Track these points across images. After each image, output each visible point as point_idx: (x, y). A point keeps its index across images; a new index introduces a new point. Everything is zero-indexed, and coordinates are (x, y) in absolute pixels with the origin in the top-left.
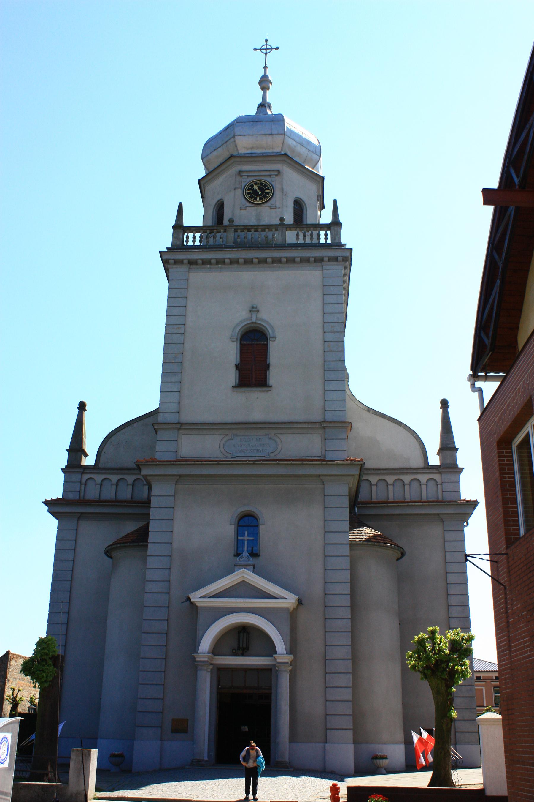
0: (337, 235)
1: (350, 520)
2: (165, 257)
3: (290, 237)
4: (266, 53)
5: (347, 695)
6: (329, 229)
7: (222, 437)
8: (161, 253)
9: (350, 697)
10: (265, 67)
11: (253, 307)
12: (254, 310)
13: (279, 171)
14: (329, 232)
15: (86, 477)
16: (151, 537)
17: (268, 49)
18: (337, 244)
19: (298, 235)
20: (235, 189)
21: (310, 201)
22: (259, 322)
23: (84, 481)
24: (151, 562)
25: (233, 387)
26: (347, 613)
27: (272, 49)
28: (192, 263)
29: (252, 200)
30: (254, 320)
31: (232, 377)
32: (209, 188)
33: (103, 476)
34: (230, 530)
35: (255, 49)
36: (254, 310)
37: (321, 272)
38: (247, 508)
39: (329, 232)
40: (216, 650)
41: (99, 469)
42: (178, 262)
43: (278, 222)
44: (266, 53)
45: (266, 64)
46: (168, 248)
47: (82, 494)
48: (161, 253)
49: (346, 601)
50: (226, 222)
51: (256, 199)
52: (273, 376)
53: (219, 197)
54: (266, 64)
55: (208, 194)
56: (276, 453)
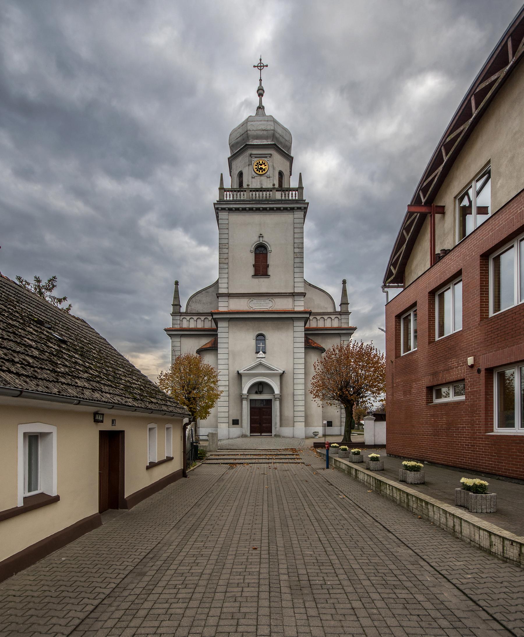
0: (301, 194)
1: (218, 343)
2: (216, 206)
3: (278, 195)
4: (261, 70)
5: (303, 409)
6: (297, 190)
7: (248, 299)
8: (214, 204)
9: (304, 410)
10: (261, 80)
11: (261, 235)
12: (261, 236)
13: (271, 155)
14: (297, 192)
15: (182, 317)
16: (219, 345)
17: (262, 66)
18: (301, 201)
19: (282, 194)
20: (249, 165)
21: (286, 173)
22: (263, 242)
23: (181, 320)
24: (220, 356)
25: (252, 276)
26: (303, 376)
27: (264, 66)
28: (230, 210)
29: (258, 172)
30: (261, 242)
31: (252, 271)
32: (234, 164)
33: (191, 317)
34: (253, 342)
35: (254, 66)
36: (261, 236)
37: (293, 216)
38: (260, 332)
39: (297, 192)
40: (250, 391)
41: (188, 313)
42: (223, 209)
43: (272, 187)
44: (261, 70)
45: (261, 78)
46: (217, 201)
47: (181, 326)
48: (214, 204)
49: (303, 371)
50: (245, 186)
51: (259, 172)
52: (270, 271)
53: (240, 170)
54: (261, 78)
55: (234, 167)
56: (249, 302)
